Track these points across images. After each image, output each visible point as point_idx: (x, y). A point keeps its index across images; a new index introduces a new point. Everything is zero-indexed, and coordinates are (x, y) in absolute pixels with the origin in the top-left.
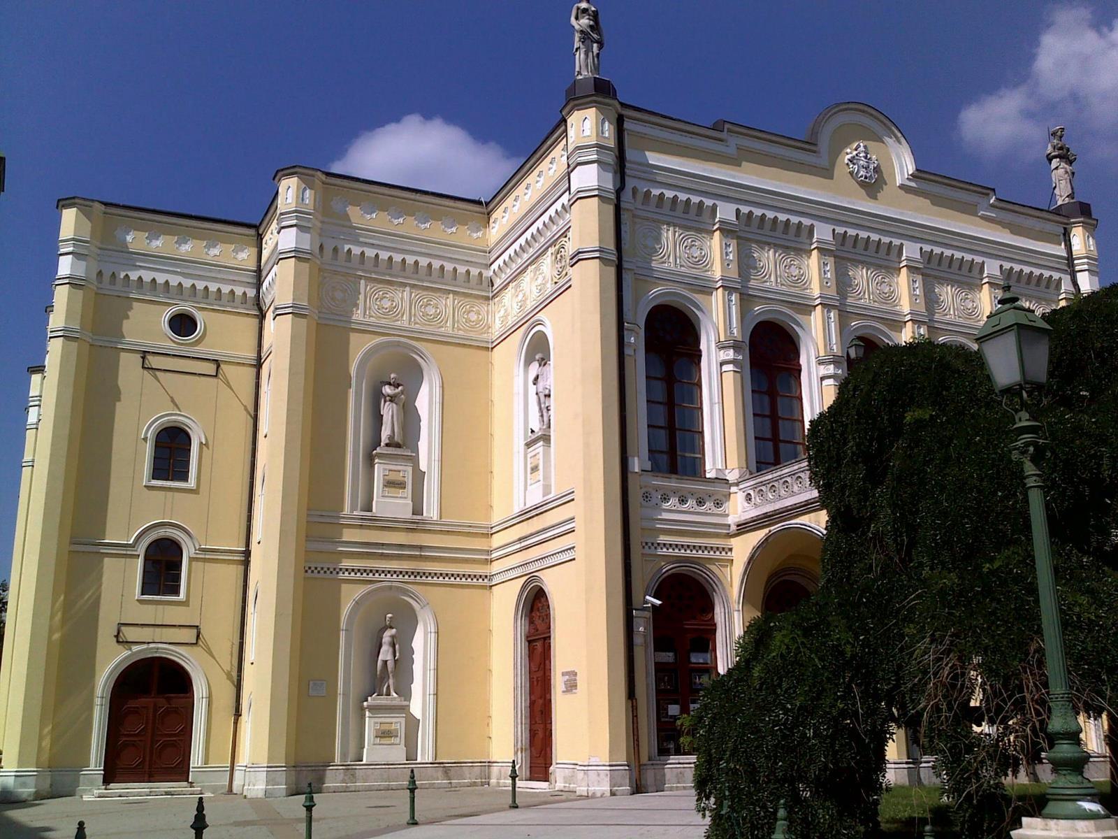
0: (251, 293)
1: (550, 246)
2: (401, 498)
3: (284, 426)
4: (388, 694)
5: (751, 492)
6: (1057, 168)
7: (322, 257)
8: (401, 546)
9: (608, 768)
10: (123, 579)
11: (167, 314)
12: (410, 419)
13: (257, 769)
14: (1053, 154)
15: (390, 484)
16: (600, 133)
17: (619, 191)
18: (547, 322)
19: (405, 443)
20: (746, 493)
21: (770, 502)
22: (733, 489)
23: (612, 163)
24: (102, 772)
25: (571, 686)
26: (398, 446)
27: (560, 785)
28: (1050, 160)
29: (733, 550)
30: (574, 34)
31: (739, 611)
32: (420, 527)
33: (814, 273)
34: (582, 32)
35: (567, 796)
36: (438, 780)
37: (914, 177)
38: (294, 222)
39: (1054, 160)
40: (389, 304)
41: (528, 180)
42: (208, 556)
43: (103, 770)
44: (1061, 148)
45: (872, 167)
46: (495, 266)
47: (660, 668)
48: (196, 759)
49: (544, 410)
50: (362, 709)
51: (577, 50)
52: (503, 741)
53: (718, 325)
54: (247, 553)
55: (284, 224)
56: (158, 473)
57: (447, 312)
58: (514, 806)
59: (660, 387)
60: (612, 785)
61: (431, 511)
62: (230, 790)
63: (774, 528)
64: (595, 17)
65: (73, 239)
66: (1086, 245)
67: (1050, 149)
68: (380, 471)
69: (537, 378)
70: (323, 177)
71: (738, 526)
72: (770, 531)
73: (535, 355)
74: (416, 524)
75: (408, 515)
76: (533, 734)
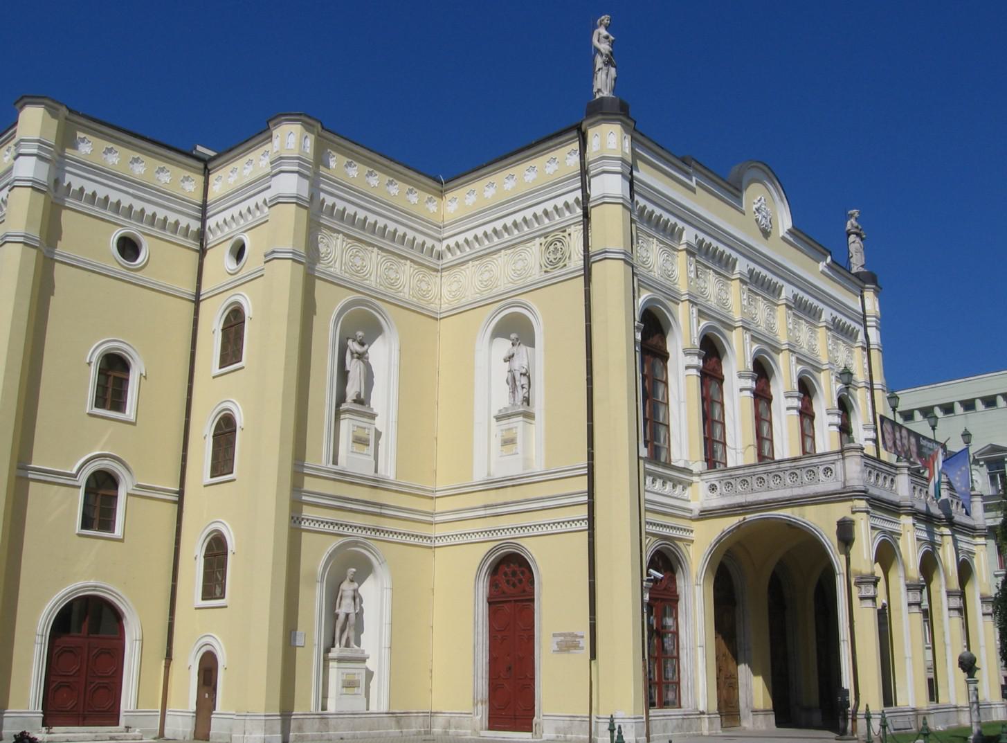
0: (195, 225)
1: (540, 236)
2: (366, 455)
3: (283, 372)
4: (347, 645)
5: (717, 484)
6: (854, 242)
7: (56, 191)
8: (366, 503)
9: (263, 718)
11: (118, 233)
13: (253, 718)
14: (852, 231)
20: (709, 484)
21: (741, 493)
22: (695, 479)
24: (42, 715)
29: (694, 532)
31: (700, 585)
36: (391, 728)
37: (790, 232)
38: (296, 168)
39: (852, 235)
40: (361, 263)
41: (251, 156)
42: (144, 493)
43: (42, 713)
48: (128, 700)
51: (599, 70)
55: (22, 151)
57: (408, 279)
62: (162, 734)
63: (750, 517)
65: (39, 141)
68: (346, 426)
70: (67, 113)
71: (701, 512)
72: (744, 519)
73: (359, 330)
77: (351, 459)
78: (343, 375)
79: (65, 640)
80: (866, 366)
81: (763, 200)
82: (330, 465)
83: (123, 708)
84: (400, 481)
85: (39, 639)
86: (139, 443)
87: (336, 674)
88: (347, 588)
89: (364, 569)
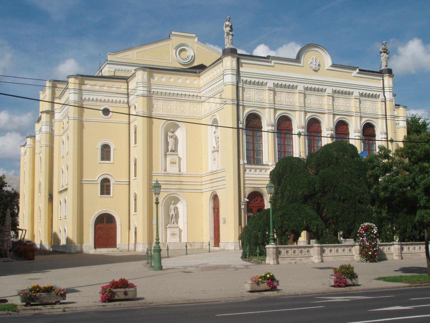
0: (126, 100)
4: (174, 223)
10: (93, 191)
12: (176, 140)
15: (172, 163)
16: (232, 65)
17: (238, 82)
18: (217, 115)
19: (175, 150)
23: (235, 73)
25: (225, 222)
26: (174, 151)
27: (222, 248)
28: (381, 53)
30: (224, 34)
32: (181, 175)
33: (296, 99)
34: (227, 33)
35: (223, 250)
38: (142, 85)
42: (118, 183)
44: (384, 49)
45: (317, 64)
46: (202, 93)
47: (249, 217)
49: (217, 142)
50: (166, 228)
52: (207, 235)
53: (268, 121)
54: (129, 182)
55: (138, 86)
56: (103, 159)
58: (210, 252)
59: (251, 138)
60: (235, 247)
61: (184, 170)
64: (231, 27)
66: (389, 83)
67: (381, 50)
68: (169, 159)
69: (215, 132)
74: (180, 175)
75: (177, 172)
76: (215, 234)
77: (172, 169)
78: (167, 143)
79: (100, 225)
80: (384, 108)
81: (314, 59)
82: (163, 172)
83: (117, 243)
84: (188, 173)
85: (91, 226)
86: (114, 169)
87: (169, 232)
88: (172, 207)
89: (177, 200)
